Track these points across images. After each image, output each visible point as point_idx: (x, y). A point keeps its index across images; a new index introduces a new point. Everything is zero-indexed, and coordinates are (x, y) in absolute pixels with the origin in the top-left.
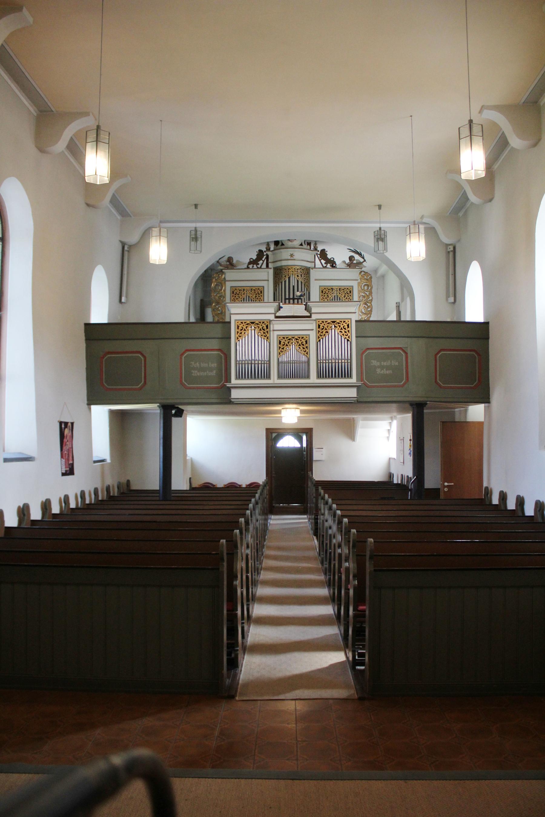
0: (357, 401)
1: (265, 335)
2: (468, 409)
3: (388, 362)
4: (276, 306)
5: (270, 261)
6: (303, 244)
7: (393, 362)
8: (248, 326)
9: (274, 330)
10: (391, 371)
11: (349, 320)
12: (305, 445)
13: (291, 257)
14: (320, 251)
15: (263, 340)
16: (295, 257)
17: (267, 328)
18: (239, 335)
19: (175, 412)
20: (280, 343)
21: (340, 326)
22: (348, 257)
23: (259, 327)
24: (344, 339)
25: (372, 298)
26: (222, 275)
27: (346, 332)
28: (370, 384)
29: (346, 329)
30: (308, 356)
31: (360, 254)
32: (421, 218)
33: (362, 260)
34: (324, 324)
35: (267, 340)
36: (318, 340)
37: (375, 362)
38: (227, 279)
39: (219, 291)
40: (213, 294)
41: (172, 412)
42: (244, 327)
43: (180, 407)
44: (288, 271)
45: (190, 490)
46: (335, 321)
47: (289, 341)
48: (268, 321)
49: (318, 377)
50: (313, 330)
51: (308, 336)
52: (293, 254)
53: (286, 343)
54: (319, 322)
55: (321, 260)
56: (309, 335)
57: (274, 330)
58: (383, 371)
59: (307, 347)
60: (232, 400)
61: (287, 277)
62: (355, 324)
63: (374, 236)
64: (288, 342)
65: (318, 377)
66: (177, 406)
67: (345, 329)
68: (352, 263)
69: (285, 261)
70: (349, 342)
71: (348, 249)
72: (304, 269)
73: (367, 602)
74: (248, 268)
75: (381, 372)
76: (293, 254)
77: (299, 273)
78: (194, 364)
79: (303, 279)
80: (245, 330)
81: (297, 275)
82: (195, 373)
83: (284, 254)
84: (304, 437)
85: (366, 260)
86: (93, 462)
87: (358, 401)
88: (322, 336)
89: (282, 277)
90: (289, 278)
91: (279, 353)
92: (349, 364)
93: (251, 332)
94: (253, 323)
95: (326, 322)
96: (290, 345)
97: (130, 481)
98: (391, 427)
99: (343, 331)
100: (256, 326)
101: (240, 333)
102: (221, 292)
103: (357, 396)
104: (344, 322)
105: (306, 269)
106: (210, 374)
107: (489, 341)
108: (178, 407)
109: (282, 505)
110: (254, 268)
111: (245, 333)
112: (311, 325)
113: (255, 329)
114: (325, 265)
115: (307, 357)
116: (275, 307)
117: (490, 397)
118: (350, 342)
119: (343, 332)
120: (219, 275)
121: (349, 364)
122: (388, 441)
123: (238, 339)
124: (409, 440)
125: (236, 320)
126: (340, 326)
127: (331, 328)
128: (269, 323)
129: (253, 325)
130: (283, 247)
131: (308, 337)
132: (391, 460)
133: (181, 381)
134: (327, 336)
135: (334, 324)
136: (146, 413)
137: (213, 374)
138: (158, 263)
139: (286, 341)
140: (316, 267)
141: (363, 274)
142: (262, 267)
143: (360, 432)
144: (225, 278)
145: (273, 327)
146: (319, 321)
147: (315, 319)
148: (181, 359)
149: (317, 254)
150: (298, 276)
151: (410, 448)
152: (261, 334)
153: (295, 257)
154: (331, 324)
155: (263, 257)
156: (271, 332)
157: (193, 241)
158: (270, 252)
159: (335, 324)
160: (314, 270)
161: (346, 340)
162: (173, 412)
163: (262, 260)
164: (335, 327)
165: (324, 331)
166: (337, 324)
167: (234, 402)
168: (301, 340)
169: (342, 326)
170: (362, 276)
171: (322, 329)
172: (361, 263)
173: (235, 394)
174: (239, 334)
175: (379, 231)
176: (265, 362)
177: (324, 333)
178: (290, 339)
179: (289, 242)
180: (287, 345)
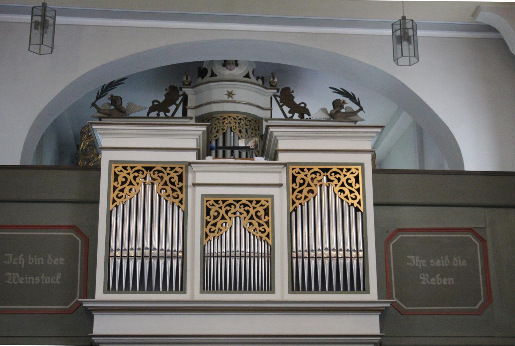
1: (175, 194)
3: (444, 259)
5: (189, 105)
6: (251, 75)
7: (455, 259)
8: (138, 176)
9: (195, 185)
10: (452, 280)
11: (360, 168)
13: (228, 98)
14: (280, 91)
15: (171, 205)
16: (235, 98)
17: (180, 179)
20: (208, 213)
21: (339, 180)
23: (162, 178)
24: (349, 206)
27: (353, 192)
30: (270, 242)
31: (352, 98)
32: (473, 16)
33: (356, 108)
34: (305, 173)
35: (179, 207)
36: (292, 208)
37: (415, 259)
39: (94, 158)
42: (130, 178)
44: (223, 123)
47: (228, 208)
48: (183, 166)
49: (293, 290)
51: (270, 200)
52: (232, 91)
53: (222, 212)
54: (293, 169)
55: (283, 105)
56: (272, 197)
57: (195, 185)
58: (433, 279)
59: (267, 223)
60: (93, 339)
61: (221, 132)
62: (373, 175)
64: (227, 212)
65: (293, 290)
68: (339, 111)
70: (359, 214)
72: (253, 120)
73: (75, 301)
74: (148, 117)
75: (429, 280)
76: (232, 91)
77: (242, 126)
78: (13, 257)
80: (131, 184)
81: (238, 129)
85: (363, 107)
90: (224, 135)
92: (361, 261)
95: (309, 170)
96: (230, 218)
99: (346, 189)
103: (381, 332)
104: (348, 170)
105: (256, 121)
111: (130, 190)
114: (289, 115)
115: (268, 243)
119: (347, 193)
121: (361, 261)
125: (111, 162)
126: (339, 180)
128: (184, 168)
130: (214, 78)
134: (312, 199)
135: (325, 174)
137: (55, 280)
139: (220, 208)
140: (273, 117)
142: (176, 116)
145: (194, 178)
146: (293, 167)
149: (275, 96)
152: (167, 194)
153: (235, 98)
155: (178, 99)
156: (190, 190)
157: (36, 28)
159: (328, 174)
161: (353, 209)
163: (176, 104)
164: (328, 180)
165: (306, 189)
166: (333, 174)
169: (343, 180)
172: (355, 113)
174: (117, 192)
175: (401, 20)
177: (305, 192)
178: (230, 205)
179: (226, 70)
180: (223, 218)
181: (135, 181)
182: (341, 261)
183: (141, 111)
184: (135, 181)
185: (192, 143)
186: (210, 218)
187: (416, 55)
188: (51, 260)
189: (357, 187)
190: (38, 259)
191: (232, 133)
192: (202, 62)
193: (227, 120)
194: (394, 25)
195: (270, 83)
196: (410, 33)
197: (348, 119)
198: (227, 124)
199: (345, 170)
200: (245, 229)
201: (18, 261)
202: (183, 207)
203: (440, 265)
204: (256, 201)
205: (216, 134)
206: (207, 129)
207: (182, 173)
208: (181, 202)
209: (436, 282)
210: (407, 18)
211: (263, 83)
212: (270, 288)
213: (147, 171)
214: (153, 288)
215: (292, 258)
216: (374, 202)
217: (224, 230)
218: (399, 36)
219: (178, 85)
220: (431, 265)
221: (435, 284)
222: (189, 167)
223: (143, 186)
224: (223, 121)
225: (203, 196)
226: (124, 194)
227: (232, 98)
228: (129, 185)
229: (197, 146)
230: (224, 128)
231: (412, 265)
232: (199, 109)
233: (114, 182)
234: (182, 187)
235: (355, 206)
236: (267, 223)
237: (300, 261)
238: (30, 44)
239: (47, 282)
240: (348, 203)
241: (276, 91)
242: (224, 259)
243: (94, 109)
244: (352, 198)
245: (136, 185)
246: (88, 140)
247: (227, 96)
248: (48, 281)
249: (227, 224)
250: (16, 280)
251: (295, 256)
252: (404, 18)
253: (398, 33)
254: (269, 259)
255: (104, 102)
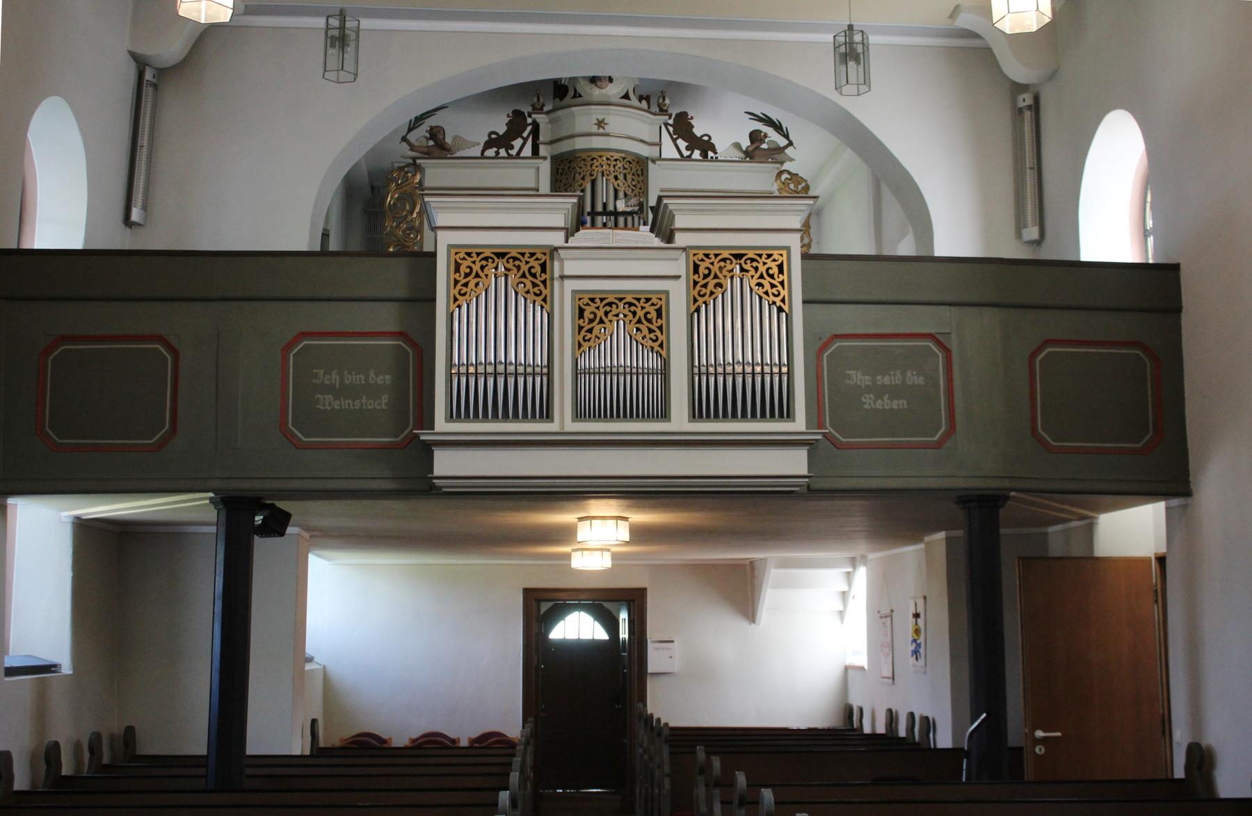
0: (808, 487)
1: (536, 290)
2: (1097, 523)
3: (895, 375)
4: (570, 206)
5: (541, 139)
7: (909, 374)
8: (487, 265)
9: (562, 277)
10: (905, 402)
11: (784, 253)
12: (624, 634)
13: (598, 129)
14: (673, 117)
15: (531, 305)
16: (608, 129)
18: (461, 290)
19: (263, 520)
20: (581, 316)
21: (756, 269)
22: (748, 135)
23: (519, 268)
24: (769, 305)
25: (811, 240)
26: (414, 175)
28: (843, 440)
29: (773, 278)
30: (664, 353)
31: (778, 127)
33: (782, 142)
34: (711, 261)
35: (542, 307)
36: (693, 308)
37: (856, 376)
38: (427, 184)
39: (406, 216)
40: (389, 224)
41: (254, 521)
42: (476, 268)
43: (282, 505)
44: (591, 165)
45: (311, 756)
46: (744, 255)
47: (608, 308)
48: (547, 252)
49: (694, 417)
50: (678, 277)
52: (604, 119)
53: (600, 313)
54: (695, 255)
55: (677, 138)
56: (667, 293)
57: (562, 277)
58: (880, 401)
59: (660, 328)
60: (434, 481)
61: (588, 179)
63: (835, 48)
64: (606, 313)
65: (694, 417)
66: (268, 502)
67: (772, 276)
68: (757, 148)
69: (581, 138)
71: (745, 112)
72: (634, 161)
74: (483, 157)
75: (875, 402)
76: (604, 119)
77: (619, 171)
78: (325, 374)
79: (629, 186)
80: (477, 276)
81: (613, 174)
82: (327, 402)
83: (581, 119)
84: (623, 616)
85: (793, 141)
86: (2, 672)
87: (812, 488)
88: (704, 295)
89: (574, 178)
91: (577, 342)
92: (785, 378)
93: (496, 281)
94: (501, 255)
95: (716, 256)
96: (611, 321)
97: (136, 728)
98: (850, 583)
99: (766, 283)
100: (509, 266)
101: (462, 285)
102: (409, 218)
103: (809, 472)
104: (769, 256)
105: (638, 162)
106: (370, 405)
107: (1183, 321)
108: (273, 505)
109: (561, 791)
110: (500, 156)
111: (477, 285)
112: (673, 263)
113: (507, 273)
114: (686, 153)
115: (661, 356)
116: (568, 209)
117: (1191, 478)
118: (787, 315)
119: (767, 287)
120: (407, 173)
121: (785, 378)
122: (842, 622)
123: (457, 303)
124: (911, 616)
125: (450, 246)
126: (756, 269)
127: (731, 274)
128: (548, 254)
129: (501, 260)
130: (578, 100)
131: (664, 299)
132: (850, 672)
133: (283, 425)
134: (720, 296)
135: (738, 261)
136: (185, 533)
137: (380, 404)
138: (205, 20)
140: (663, 157)
141: (787, 179)
142: (522, 155)
143: (770, 598)
144: (421, 183)
145: (562, 268)
146: (695, 252)
147: (683, 245)
148: (285, 359)
149: (666, 125)
150: (616, 178)
151: (916, 638)
152: (526, 289)
153: (608, 129)
154: (731, 263)
155: (526, 129)
156: (556, 284)
157: (333, 46)
158: (544, 116)
159: (742, 261)
160: (659, 165)
162: (259, 519)
163: (522, 138)
164: (742, 270)
165: (712, 283)
166: (748, 262)
167: (441, 488)
168: (644, 305)
169: (762, 269)
170: (783, 183)
171: (706, 276)
173: (446, 464)
174: (459, 287)
175: (847, 32)
176: (536, 368)
177: (711, 287)
178: (610, 304)
179: (595, 88)
180: (601, 321)
181: (483, 272)
182: (758, 379)
183: (473, 148)
184: (483, 272)
185: (559, 220)
186: (584, 322)
187: (867, 81)
188: (374, 377)
189: (780, 280)
190: (358, 376)
191: (604, 178)
192: (561, 79)
193: (598, 161)
194: (836, 37)
195: (659, 106)
196: (860, 49)
197: (772, 159)
198: (597, 167)
199: (764, 256)
200: (631, 337)
201: (330, 380)
202: (547, 307)
203: (888, 383)
204: (645, 298)
205: (581, 181)
206: (579, 201)
207: (545, 260)
208: (544, 300)
209: (883, 405)
210: (855, 28)
211: (649, 108)
212: (665, 415)
213: (499, 259)
214: (511, 415)
215: (693, 374)
216: (803, 299)
217: (603, 338)
218: (843, 53)
219: (526, 109)
220: (878, 383)
221: (881, 408)
222: (555, 252)
223: (493, 279)
224: (592, 162)
225: (574, 292)
226: (469, 290)
227: (604, 129)
228: (475, 277)
229: (565, 224)
230: (593, 173)
231: (852, 383)
232: (555, 145)
233: (455, 273)
234: (546, 280)
235: (778, 305)
236: (660, 328)
237: (704, 378)
238: (325, 70)
239: (369, 407)
240: (769, 302)
241: (667, 117)
242: (603, 377)
243: (405, 146)
244: (774, 295)
245: (484, 277)
246: (398, 191)
247: (596, 126)
248: (370, 405)
249: (607, 330)
250: (330, 404)
251: (697, 372)
252: (851, 27)
253: (843, 49)
254: (663, 376)
255: (421, 132)
